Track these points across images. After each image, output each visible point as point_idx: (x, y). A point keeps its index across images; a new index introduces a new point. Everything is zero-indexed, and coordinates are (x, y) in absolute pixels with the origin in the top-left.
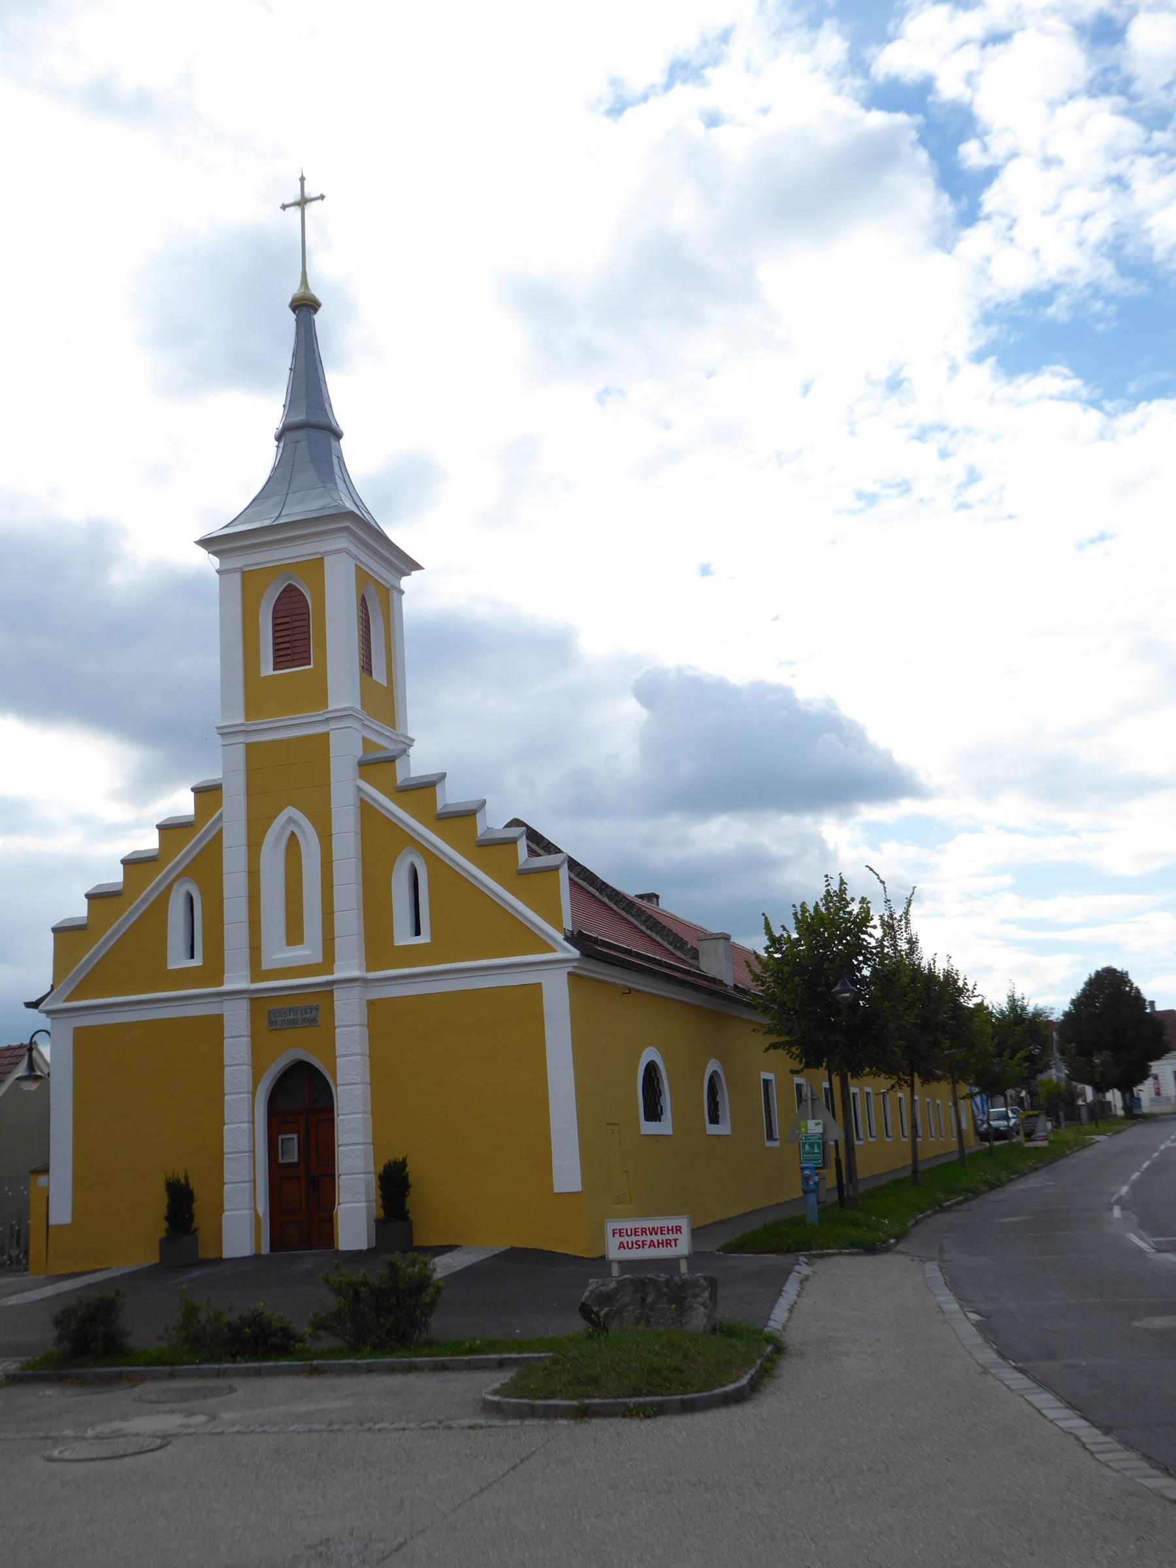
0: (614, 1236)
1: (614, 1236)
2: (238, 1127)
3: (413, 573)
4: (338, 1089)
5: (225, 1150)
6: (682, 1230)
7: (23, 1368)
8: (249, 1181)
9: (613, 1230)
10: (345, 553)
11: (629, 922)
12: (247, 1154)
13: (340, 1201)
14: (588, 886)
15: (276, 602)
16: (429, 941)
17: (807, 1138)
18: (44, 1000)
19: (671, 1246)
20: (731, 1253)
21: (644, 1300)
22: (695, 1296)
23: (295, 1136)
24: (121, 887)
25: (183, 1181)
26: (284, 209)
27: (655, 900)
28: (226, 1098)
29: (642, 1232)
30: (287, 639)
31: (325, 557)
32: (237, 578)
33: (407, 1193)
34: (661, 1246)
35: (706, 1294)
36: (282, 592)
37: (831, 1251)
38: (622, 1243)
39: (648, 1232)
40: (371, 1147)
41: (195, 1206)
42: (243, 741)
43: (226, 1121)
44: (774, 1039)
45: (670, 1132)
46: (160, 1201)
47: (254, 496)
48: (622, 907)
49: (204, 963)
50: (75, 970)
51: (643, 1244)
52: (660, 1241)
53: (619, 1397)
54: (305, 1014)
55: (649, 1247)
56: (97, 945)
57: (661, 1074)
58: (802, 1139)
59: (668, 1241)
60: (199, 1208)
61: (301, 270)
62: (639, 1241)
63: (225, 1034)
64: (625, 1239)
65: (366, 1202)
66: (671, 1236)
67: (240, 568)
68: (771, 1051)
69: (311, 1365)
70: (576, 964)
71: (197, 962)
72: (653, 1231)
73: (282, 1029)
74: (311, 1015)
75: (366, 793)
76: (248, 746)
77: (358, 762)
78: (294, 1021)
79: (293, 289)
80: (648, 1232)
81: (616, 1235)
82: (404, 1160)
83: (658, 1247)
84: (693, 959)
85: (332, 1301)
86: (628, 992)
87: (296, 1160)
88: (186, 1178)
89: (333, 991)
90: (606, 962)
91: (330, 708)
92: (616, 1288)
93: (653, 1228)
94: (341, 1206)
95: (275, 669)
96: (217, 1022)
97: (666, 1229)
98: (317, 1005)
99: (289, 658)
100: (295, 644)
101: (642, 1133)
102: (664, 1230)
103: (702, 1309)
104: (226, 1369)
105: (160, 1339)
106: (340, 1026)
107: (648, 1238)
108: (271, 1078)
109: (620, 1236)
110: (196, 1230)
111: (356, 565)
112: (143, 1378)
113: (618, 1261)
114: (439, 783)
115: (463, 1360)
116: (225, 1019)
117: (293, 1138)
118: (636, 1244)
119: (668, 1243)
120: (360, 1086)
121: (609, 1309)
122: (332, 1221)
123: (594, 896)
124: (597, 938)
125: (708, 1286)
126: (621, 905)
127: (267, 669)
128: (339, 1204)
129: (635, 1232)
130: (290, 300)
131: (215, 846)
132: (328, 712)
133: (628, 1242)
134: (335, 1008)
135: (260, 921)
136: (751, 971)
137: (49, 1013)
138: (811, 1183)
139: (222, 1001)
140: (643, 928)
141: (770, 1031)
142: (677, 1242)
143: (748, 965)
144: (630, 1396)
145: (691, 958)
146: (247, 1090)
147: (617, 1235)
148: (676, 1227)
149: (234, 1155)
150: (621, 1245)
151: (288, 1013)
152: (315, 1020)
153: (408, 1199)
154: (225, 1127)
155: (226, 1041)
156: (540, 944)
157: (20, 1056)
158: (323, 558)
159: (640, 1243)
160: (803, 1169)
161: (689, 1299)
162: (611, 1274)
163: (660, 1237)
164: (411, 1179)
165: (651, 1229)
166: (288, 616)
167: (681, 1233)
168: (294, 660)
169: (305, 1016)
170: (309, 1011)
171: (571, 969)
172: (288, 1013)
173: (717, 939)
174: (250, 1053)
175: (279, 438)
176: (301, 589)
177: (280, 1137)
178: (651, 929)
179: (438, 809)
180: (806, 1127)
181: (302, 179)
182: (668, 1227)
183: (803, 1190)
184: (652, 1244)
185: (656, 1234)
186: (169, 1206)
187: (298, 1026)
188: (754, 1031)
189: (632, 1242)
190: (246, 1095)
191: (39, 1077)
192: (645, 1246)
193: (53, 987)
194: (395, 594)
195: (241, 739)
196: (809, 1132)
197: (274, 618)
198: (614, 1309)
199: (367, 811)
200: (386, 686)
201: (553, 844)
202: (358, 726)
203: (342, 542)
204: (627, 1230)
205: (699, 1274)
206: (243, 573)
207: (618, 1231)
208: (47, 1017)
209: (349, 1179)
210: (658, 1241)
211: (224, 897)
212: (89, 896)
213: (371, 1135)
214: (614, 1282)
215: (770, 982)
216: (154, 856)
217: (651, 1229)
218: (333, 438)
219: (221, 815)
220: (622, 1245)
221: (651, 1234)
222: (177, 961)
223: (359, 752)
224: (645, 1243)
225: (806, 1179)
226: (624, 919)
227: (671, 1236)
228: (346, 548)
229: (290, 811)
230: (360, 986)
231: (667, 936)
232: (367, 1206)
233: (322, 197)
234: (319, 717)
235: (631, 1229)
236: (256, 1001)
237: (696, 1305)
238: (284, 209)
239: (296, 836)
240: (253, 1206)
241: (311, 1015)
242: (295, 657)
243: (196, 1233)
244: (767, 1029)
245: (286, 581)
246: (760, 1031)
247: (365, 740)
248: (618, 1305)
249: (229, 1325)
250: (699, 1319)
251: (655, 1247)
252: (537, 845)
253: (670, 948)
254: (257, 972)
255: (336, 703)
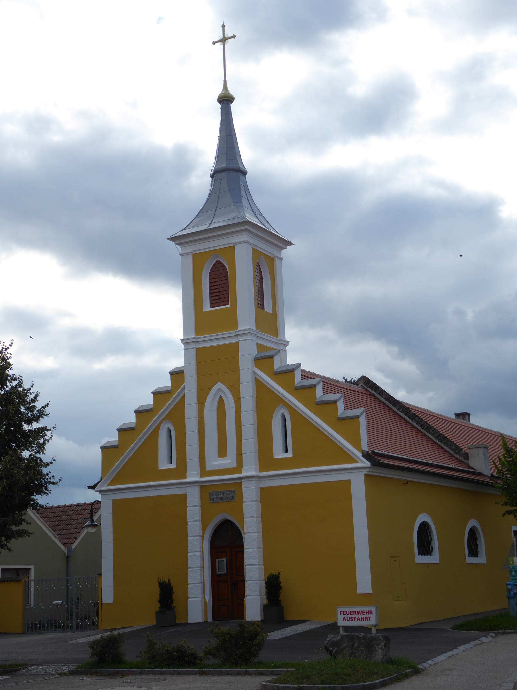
0: (341, 615)
1: (341, 615)
2: (195, 554)
3: (288, 247)
4: (245, 535)
5: (189, 566)
6: (373, 613)
7: (76, 668)
8: (201, 583)
9: (341, 612)
10: (245, 243)
11: (429, 438)
12: (200, 569)
13: (247, 595)
14: (405, 416)
15: (211, 270)
16: (292, 456)
17: (513, 567)
18: (100, 482)
19: (367, 620)
20: (455, 630)
21: (353, 645)
22: (378, 645)
23: (225, 560)
24: (135, 425)
25: (167, 582)
26: (214, 44)
27: (467, 417)
28: (189, 538)
29: (354, 613)
30: (217, 290)
31: (235, 246)
32: (190, 258)
33: (280, 592)
34: (363, 620)
35: (383, 644)
36: (214, 265)
37: (510, 631)
38: (344, 618)
39: (357, 613)
40: (263, 566)
41: (173, 595)
42: (194, 347)
43: (189, 551)
44: (509, 508)
45: (438, 562)
46: (156, 591)
47: (199, 212)
48: (424, 428)
49: (177, 466)
50: (113, 469)
51: (354, 619)
52: (363, 618)
53: (315, 684)
54: (228, 495)
55: (357, 620)
56: (123, 456)
57: (431, 528)
58: (510, 568)
59: (366, 618)
60: (177, 595)
61: (223, 79)
62: (352, 617)
63: (187, 504)
64: (346, 616)
65: (260, 595)
66: (367, 615)
67: (192, 252)
68: (507, 516)
69: (202, 670)
70: (368, 470)
71: (174, 466)
72: (359, 613)
73: (216, 502)
74: (231, 495)
75: (258, 375)
76: (197, 349)
77: (254, 358)
78: (222, 498)
79: (219, 91)
80: (357, 613)
81: (341, 614)
82: (279, 574)
83: (362, 620)
84: (466, 459)
85: (215, 642)
86: (407, 483)
87: (225, 572)
88: (169, 580)
89: (241, 482)
90: (386, 468)
91: (239, 329)
92: (340, 639)
93: (359, 611)
94: (247, 597)
95: (211, 307)
96: (184, 497)
97: (365, 612)
98: (234, 490)
99: (217, 301)
100: (221, 293)
101: (416, 562)
102: (364, 613)
103: (381, 651)
104: (165, 671)
105: (138, 657)
106: (245, 502)
107: (357, 616)
108: (213, 527)
109: (344, 614)
110: (174, 608)
111: (252, 248)
112: (128, 675)
113: (343, 627)
114: (296, 369)
115: (270, 671)
116: (188, 496)
117: (224, 561)
118: (351, 618)
119: (366, 619)
120: (256, 534)
121: (337, 649)
122: (243, 605)
123: (408, 422)
124: (385, 454)
125: (383, 640)
126: (424, 427)
127: (207, 308)
128: (246, 597)
129: (351, 613)
130: (217, 98)
131: (181, 403)
132: (237, 331)
133: (347, 618)
134: (243, 492)
135: (204, 444)
136: (496, 467)
137: (100, 492)
138: (512, 593)
139: (186, 487)
140: (436, 441)
141: (506, 504)
142: (371, 618)
143: (495, 464)
144: (321, 684)
145: (464, 459)
146: (199, 535)
147: (342, 614)
148: (370, 611)
149: (193, 569)
150: (344, 619)
151: (219, 494)
152: (233, 498)
153: (281, 594)
154: (189, 554)
155: (188, 509)
156: (350, 458)
157: (98, 508)
158: (234, 246)
159: (353, 618)
160: (508, 585)
161: (375, 646)
162: (339, 633)
163: (362, 616)
164: (282, 585)
165: (358, 611)
166: (217, 278)
167: (372, 614)
168: (220, 302)
169: (228, 496)
170: (230, 493)
171: (366, 473)
172: (219, 494)
173: (479, 448)
174: (200, 515)
175: (212, 177)
176: (224, 263)
177: (217, 560)
178: (441, 441)
179: (296, 383)
180: (513, 561)
181: (223, 26)
182: (366, 611)
183: (507, 597)
184: (344, 619)
185: (361, 614)
186: (160, 595)
187: (225, 501)
188: (496, 503)
189: (349, 618)
190: (199, 537)
191: (96, 526)
192: (355, 620)
193: (102, 478)
194: (277, 261)
195: (193, 346)
196: (515, 564)
197: (210, 279)
198: (340, 649)
199: (259, 385)
200: (272, 313)
201: (385, 391)
202: (254, 338)
203: (244, 237)
204: (347, 611)
205: (380, 634)
206: (194, 255)
207: (343, 612)
208: (99, 494)
209: (251, 583)
210: (361, 617)
211: (186, 432)
212: (137, 412)
213: (263, 560)
214: (339, 636)
215: (507, 474)
216: (151, 409)
217: (358, 611)
218: (240, 174)
219: (184, 387)
220: (358, 619)
221: (358, 614)
222: (164, 465)
223: (254, 352)
224: (355, 618)
225: (509, 591)
226: (426, 435)
227: (367, 615)
228: (247, 241)
229: (219, 385)
230: (256, 480)
231: (450, 445)
232: (260, 598)
233: (214, 43)
234: (234, 334)
235: (349, 611)
236: (203, 487)
237: (377, 649)
238: (214, 44)
239: (222, 398)
240: (203, 596)
241: (231, 495)
242: (221, 300)
243: (175, 609)
244: (504, 502)
245: (216, 258)
246: (499, 503)
247: (259, 346)
248: (341, 647)
249: (168, 651)
250: (379, 655)
251: (360, 620)
252: (375, 392)
253: (452, 453)
254: (204, 472)
255: (242, 327)
